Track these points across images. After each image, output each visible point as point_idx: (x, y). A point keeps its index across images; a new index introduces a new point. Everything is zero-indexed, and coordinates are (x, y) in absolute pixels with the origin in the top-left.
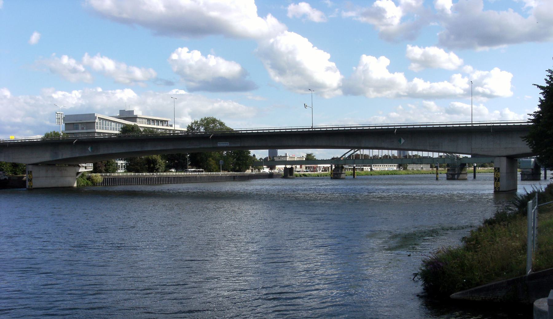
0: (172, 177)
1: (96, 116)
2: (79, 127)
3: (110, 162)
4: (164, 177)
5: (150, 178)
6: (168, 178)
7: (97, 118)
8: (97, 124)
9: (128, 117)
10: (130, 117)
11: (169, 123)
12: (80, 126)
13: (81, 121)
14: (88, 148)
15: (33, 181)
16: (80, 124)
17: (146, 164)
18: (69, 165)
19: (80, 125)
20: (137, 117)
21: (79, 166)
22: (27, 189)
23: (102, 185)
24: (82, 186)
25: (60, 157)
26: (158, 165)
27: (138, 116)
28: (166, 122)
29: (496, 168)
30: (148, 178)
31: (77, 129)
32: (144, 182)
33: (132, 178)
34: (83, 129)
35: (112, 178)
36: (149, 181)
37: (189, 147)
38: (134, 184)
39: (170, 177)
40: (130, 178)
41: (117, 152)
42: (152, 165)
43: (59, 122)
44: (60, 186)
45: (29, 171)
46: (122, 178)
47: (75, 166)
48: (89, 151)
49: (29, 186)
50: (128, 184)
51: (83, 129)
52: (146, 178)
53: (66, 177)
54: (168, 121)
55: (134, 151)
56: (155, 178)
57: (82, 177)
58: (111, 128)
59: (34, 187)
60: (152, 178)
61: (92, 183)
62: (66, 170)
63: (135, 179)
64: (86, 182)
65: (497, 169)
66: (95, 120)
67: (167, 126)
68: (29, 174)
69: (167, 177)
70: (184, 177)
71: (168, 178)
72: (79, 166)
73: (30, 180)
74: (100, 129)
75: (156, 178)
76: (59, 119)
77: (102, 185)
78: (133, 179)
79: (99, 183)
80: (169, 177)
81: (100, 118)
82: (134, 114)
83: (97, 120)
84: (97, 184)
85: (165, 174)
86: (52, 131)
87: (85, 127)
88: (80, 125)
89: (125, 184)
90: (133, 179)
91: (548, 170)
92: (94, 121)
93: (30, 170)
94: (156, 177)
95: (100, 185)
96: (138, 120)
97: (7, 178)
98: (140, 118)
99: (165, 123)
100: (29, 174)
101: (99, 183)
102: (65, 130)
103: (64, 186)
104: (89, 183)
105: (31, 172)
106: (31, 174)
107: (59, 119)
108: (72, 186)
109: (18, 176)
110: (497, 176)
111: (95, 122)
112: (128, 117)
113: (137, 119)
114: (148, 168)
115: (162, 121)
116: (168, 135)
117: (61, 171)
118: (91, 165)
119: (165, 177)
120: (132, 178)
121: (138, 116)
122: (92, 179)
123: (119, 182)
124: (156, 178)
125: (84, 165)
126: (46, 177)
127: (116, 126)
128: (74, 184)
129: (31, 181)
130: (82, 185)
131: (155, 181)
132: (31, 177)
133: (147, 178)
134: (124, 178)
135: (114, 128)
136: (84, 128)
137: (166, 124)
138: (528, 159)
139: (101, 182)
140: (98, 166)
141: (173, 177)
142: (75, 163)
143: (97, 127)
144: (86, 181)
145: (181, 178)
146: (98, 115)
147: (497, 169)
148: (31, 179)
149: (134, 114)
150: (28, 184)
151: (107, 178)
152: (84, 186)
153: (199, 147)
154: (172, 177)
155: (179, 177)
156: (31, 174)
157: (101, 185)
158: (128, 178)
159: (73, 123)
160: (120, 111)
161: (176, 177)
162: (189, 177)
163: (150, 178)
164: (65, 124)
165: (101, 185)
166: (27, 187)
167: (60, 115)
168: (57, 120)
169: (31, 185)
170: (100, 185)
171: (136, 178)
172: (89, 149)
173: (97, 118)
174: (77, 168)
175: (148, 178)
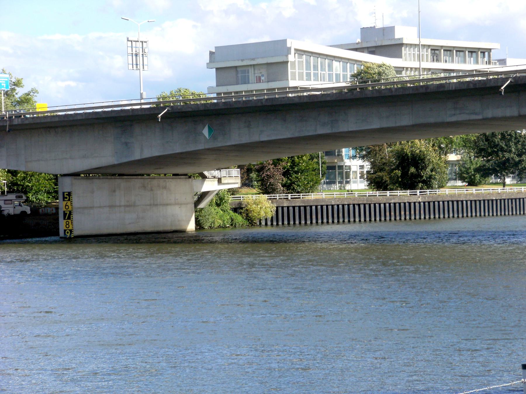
0: (467, 201)
1: (288, 45)
2: (248, 76)
3: (298, 164)
4: (443, 202)
5: (405, 203)
6: (455, 203)
7: (293, 51)
8: (293, 67)
9: (380, 45)
10: (384, 44)
11: (494, 56)
12: (252, 75)
13: (253, 59)
14: (204, 128)
15: (75, 217)
16: (253, 69)
17: (397, 168)
18: (174, 175)
19: (251, 70)
20: (402, 45)
21: (204, 177)
22: (61, 238)
23: (275, 223)
24: (219, 227)
25: (137, 156)
26: (428, 170)
27: (404, 42)
28: (486, 54)
29: (65, 194)
30: (397, 205)
31: (246, 81)
32: (388, 214)
33: (354, 205)
34: (259, 80)
35: (300, 207)
36: (403, 213)
37: (453, 119)
38: (516, 214)
39: (462, 201)
40: (349, 205)
41: (273, 138)
42: (412, 170)
43: (137, 65)
44: (149, 229)
45: (64, 193)
46: (434, 202)
47: (190, 177)
48: (205, 136)
49: (65, 231)
50: (344, 221)
51: (260, 82)
52: (392, 205)
53: (167, 205)
54: (490, 50)
55: (315, 133)
56: (420, 203)
57: (218, 205)
58: (330, 76)
59: (76, 233)
60: (410, 203)
61: (246, 219)
62: (165, 188)
63: (362, 207)
64: (228, 217)
65: (66, 195)
66: (287, 56)
67: (489, 62)
68: (64, 200)
69: (453, 202)
70: (504, 200)
71: (455, 203)
72: (204, 177)
73: (68, 216)
74: (301, 78)
75: (422, 204)
76: (136, 55)
77: (275, 223)
78: (357, 207)
79: (266, 220)
80: (457, 201)
81: (300, 52)
82: (396, 37)
83: (291, 58)
84: (260, 223)
85: (474, 192)
86: (174, 89)
87: (263, 76)
88: (251, 70)
89: (336, 221)
90: (357, 207)
91: (193, 231)
92: (285, 60)
93: (67, 190)
94: (420, 200)
95: (269, 223)
96: (405, 51)
97: (29, 212)
98: (411, 45)
99: (484, 57)
100: (64, 200)
101: (266, 220)
102: (217, 85)
103: (161, 229)
104: (239, 219)
105: (69, 194)
106: (69, 200)
107: (136, 55)
108: (182, 228)
109: (312, 197)
110: (67, 207)
111: (287, 62)
112: (379, 44)
113: (403, 48)
114: (402, 176)
115: (473, 51)
116: (383, 87)
117: (152, 190)
118: (235, 172)
119: (448, 202)
120: (354, 205)
121: (405, 42)
122: (247, 210)
123: (491, 211)
124: (422, 204)
125: (216, 173)
126: (111, 206)
127: (345, 69)
128: (188, 223)
129: (69, 218)
130: (217, 225)
131: (417, 212)
132: (70, 209)
133: (395, 204)
134: (333, 206)
135: (338, 76)
136: (263, 78)
137: (486, 59)
138: (463, 74)
139: (269, 216)
140: (268, 175)
141: (471, 201)
142: (189, 170)
143: (294, 74)
144: (229, 214)
145: (495, 202)
146: (293, 44)
147: (66, 195)
148: (70, 213)
149: (396, 37)
150: (62, 224)
151: (288, 207)
152: (225, 227)
153: (480, 117)
154: (467, 201)
155: (488, 201)
156: (69, 200)
157: (272, 224)
158: (343, 206)
159: (236, 67)
160: (363, 30)
161: (480, 201)
162: (520, 199)
163: (405, 203)
164: (217, 69)
165: (272, 224)
166: (62, 234)
167: (139, 45)
168: (130, 57)
169: (70, 228)
170: (269, 223)
171: (448, 202)
172: (206, 132)
173: (293, 51)
174: (195, 182)
175: (400, 204)
